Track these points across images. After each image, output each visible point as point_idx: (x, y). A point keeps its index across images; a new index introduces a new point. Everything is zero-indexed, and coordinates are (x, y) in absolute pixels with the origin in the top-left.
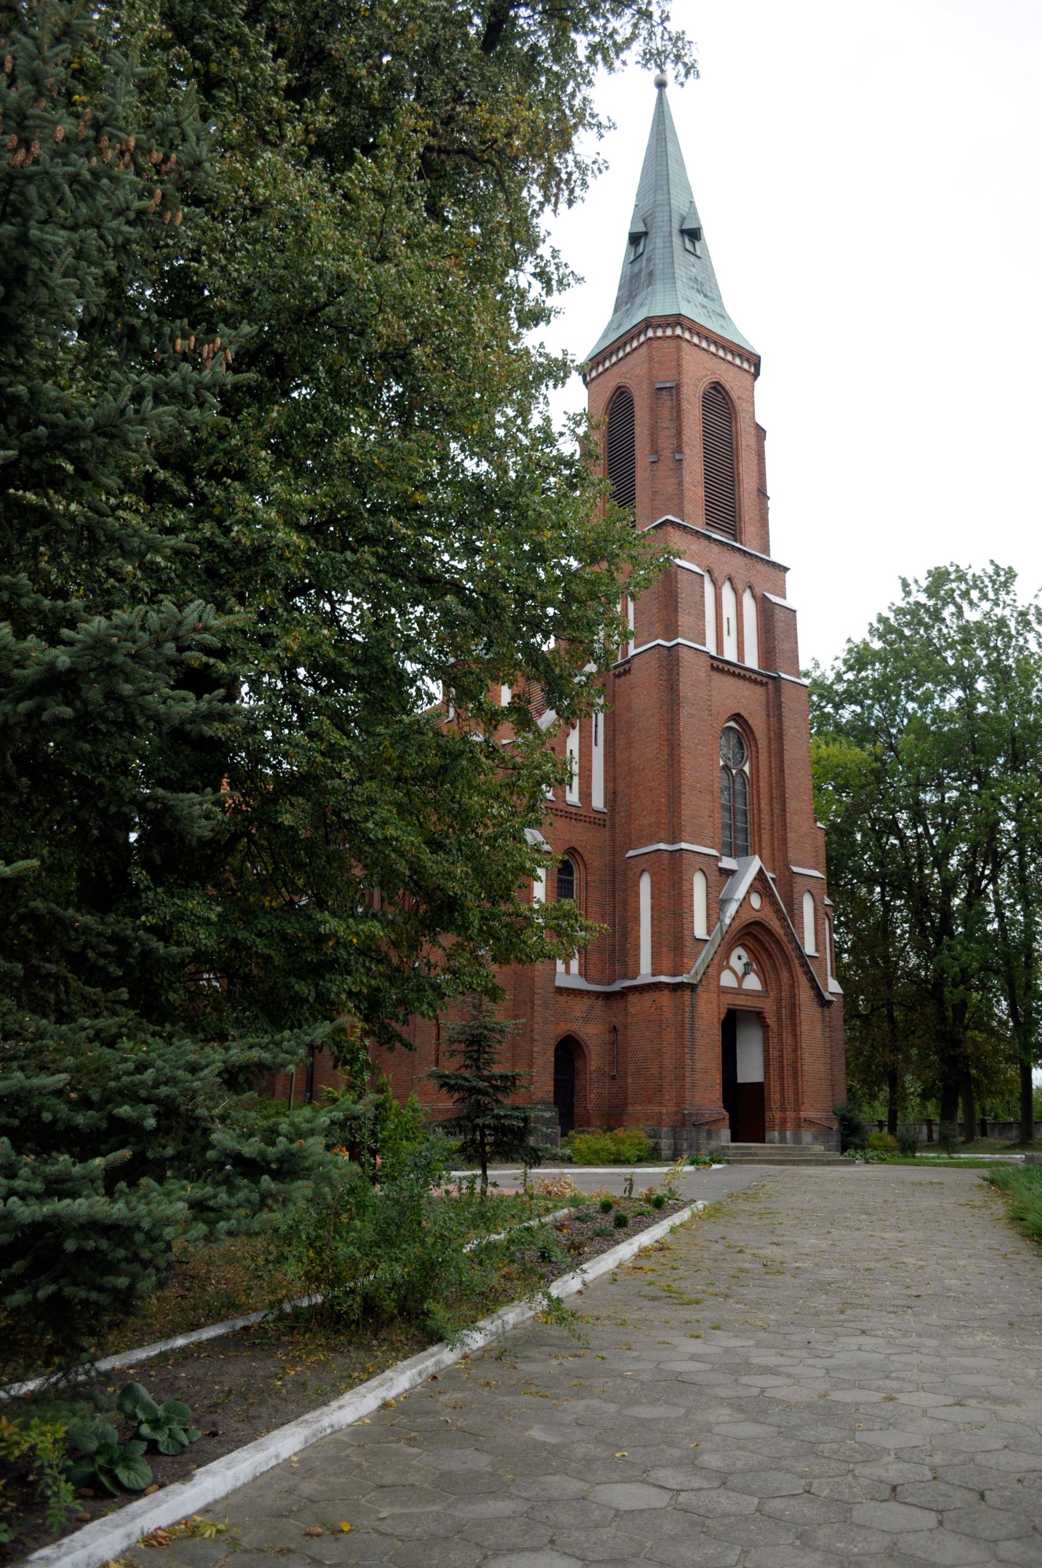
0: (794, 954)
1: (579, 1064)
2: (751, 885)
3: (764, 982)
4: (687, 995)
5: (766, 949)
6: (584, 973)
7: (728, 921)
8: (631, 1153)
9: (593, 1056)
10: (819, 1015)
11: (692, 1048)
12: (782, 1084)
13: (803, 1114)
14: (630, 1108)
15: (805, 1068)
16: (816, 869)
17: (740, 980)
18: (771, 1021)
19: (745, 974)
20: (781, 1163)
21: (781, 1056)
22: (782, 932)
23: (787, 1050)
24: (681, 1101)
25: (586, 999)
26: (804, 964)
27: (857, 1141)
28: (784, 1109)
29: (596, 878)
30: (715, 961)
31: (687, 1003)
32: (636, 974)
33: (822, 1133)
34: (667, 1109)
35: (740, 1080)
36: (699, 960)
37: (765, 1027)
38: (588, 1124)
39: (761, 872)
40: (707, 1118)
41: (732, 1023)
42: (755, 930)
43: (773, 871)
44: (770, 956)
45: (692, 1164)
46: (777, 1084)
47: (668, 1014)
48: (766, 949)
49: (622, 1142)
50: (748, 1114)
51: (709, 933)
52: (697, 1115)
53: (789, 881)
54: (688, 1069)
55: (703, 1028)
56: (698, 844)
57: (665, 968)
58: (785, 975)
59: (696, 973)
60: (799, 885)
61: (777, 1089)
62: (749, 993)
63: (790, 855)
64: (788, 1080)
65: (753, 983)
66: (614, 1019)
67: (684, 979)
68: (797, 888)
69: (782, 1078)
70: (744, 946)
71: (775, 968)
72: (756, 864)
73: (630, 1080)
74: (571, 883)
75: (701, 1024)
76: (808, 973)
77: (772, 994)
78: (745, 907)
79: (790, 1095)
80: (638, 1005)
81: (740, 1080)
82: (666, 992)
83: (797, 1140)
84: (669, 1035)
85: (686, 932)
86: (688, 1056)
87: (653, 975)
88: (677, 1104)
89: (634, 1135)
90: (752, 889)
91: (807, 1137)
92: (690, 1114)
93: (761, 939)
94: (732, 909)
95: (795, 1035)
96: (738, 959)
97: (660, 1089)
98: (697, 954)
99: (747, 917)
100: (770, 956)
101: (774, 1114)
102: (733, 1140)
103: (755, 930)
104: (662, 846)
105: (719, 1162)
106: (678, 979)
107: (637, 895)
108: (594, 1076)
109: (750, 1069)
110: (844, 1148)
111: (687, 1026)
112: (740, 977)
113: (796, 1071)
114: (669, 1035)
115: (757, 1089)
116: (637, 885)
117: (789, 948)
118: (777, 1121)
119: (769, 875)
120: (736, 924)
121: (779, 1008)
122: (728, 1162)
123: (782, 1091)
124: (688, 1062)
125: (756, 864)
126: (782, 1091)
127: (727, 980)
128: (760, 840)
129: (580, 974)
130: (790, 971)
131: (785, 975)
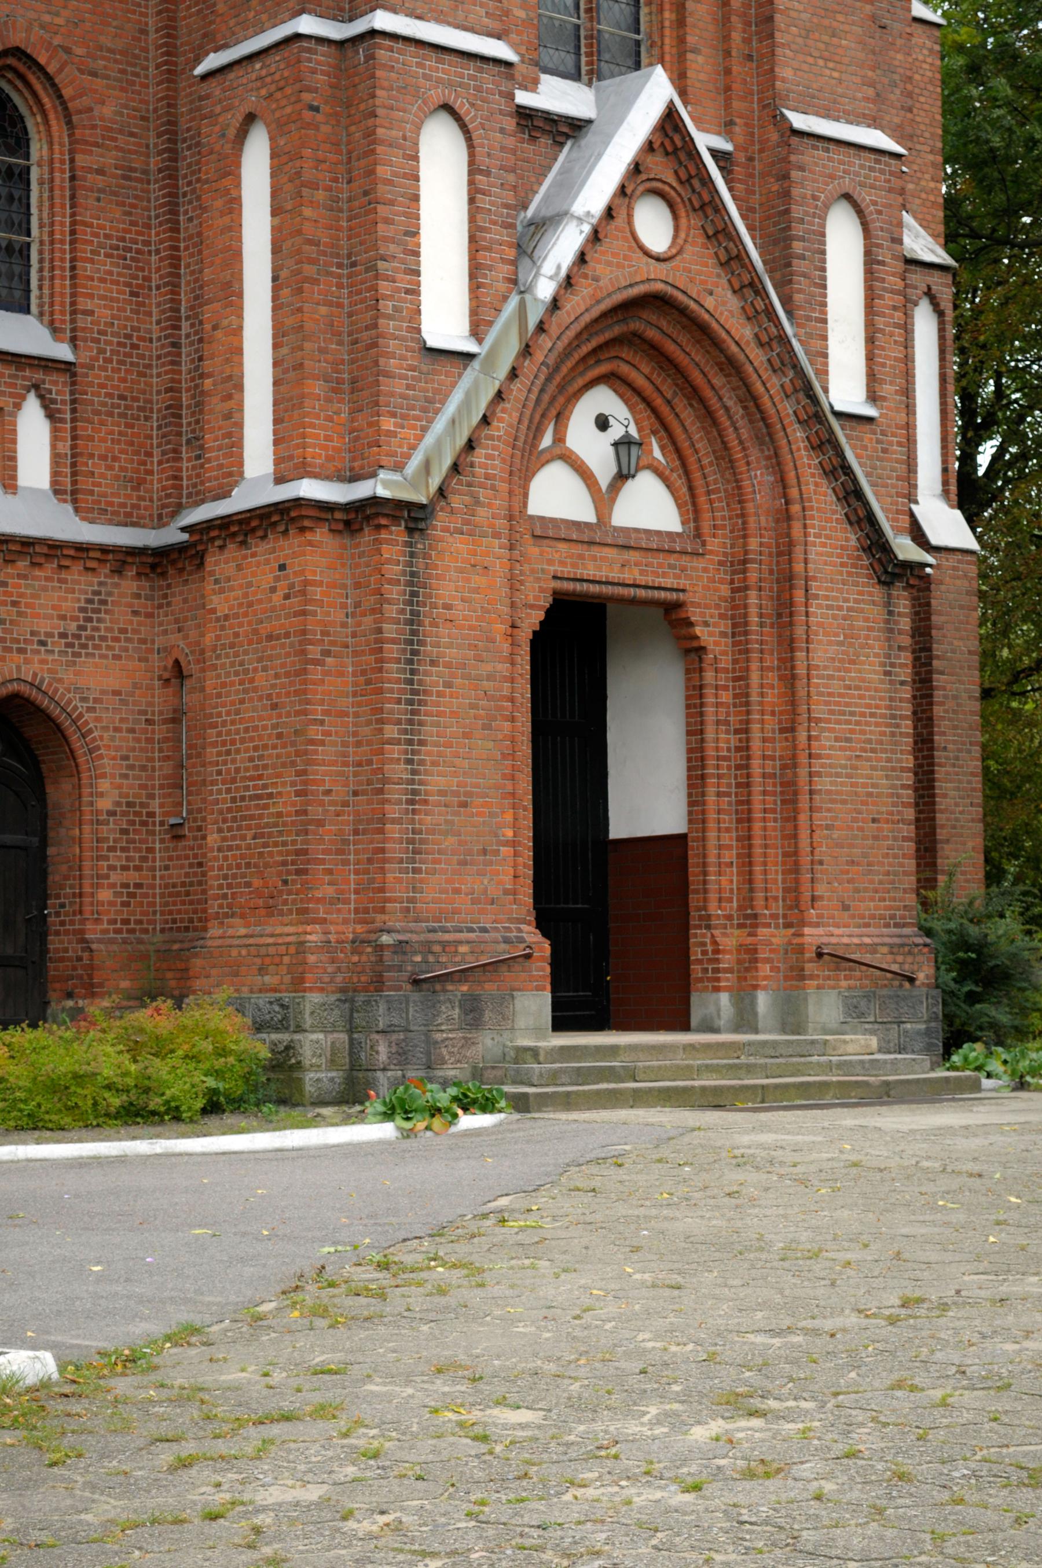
0: (788, 408)
1: (58, 793)
2: (636, 168)
3: (690, 504)
4: (393, 543)
5: (694, 395)
6: (70, 485)
7: (545, 289)
8: (181, 1081)
9: (107, 764)
10: (877, 612)
11: (413, 722)
12: (746, 839)
13: (813, 936)
14: (214, 931)
15: (823, 784)
16: (874, 122)
17: (604, 499)
18: (711, 633)
19: (622, 477)
20: (716, 1100)
21: (744, 749)
22: (745, 332)
23: (764, 728)
24: (373, 900)
25: (75, 574)
26: (825, 444)
27: (1003, 1016)
28: (750, 921)
29: (109, 160)
30: (500, 428)
31: (393, 570)
32: (232, 474)
33: (877, 989)
34: (323, 932)
35: (617, 830)
36: (440, 425)
37: (693, 653)
38: (92, 991)
39: (670, 119)
40: (465, 957)
41: (574, 650)
42: (650, 326)
43: (726, 129)
44: (708, 415)
45: (388, 1115)
46: (729, 839)
47: (330, 611)
48: (694, 395)
49: (161, 1049)
50: (615, 934)
51: (477, 331)
52: (427, 947)
53: (774, 161)
54: (395, 793)
55: (451, 654)
56: (441, 18)
57: (316, 454)
58: (758, 479)
59: (427, 467)
60: (811, 173)
61: (730, 856)
62: (633, 542)
63: (784, 72)
64: (766, 828)
65: (649, 506)
66: (174, 639)
67: (382, 486)
68: (805, 185)
69: (745, 819)
70: (613, 380)
71: (724, 454)
72: (655, 92)
73: (213, 839)
74: (23, 176)
75: (445, 643)
76: (839, 470)
77: (714, 544)
78: (614, 244)
79: (772, 875)
80: (238, 579)
81: (617, 830)
82: (321, 535)
83: (792, 1020)
84: (334, 683)
85: (389, 326)
86: (395, 752)
87: (280, 479)
88: (363, 914)
89: (216, 1022)
90: (636, 182)
91: (825, 1006)
92: (401, 947)
93: (663, 352)
94: (563, 248)
95: (789, 679)
96: (595, 424)
97: (300, 865)
98: (432, 406)
99: (615, 279)
100: (708, 415)
101: (717, 935)
102: (559, 1025)
103: (650, 326)
104: (307, 25)
105: (487, 1106)
106: (362, 490)
107: (234, 205)
108: (110, 831)
109: (646, 795)
110: (953, 1038)
111: (392, 650)
112: (600, 486)
113: (789, 796)
114: (334, 683)
115: (669, 854)
116: (231, 171)
117: (772, 388)
118: (727, 960)
119: (704, 141)
120: (580, 305)
121: (740, 589)
122: (521, 1104)
123: (747, 861)
124: (398, 771)
125: (655, 92)
126: (747, 861)
127: (555, 496)
128: (681, 23)
129: (57, 490)
130: (777, 464)
131: (758, 479)
